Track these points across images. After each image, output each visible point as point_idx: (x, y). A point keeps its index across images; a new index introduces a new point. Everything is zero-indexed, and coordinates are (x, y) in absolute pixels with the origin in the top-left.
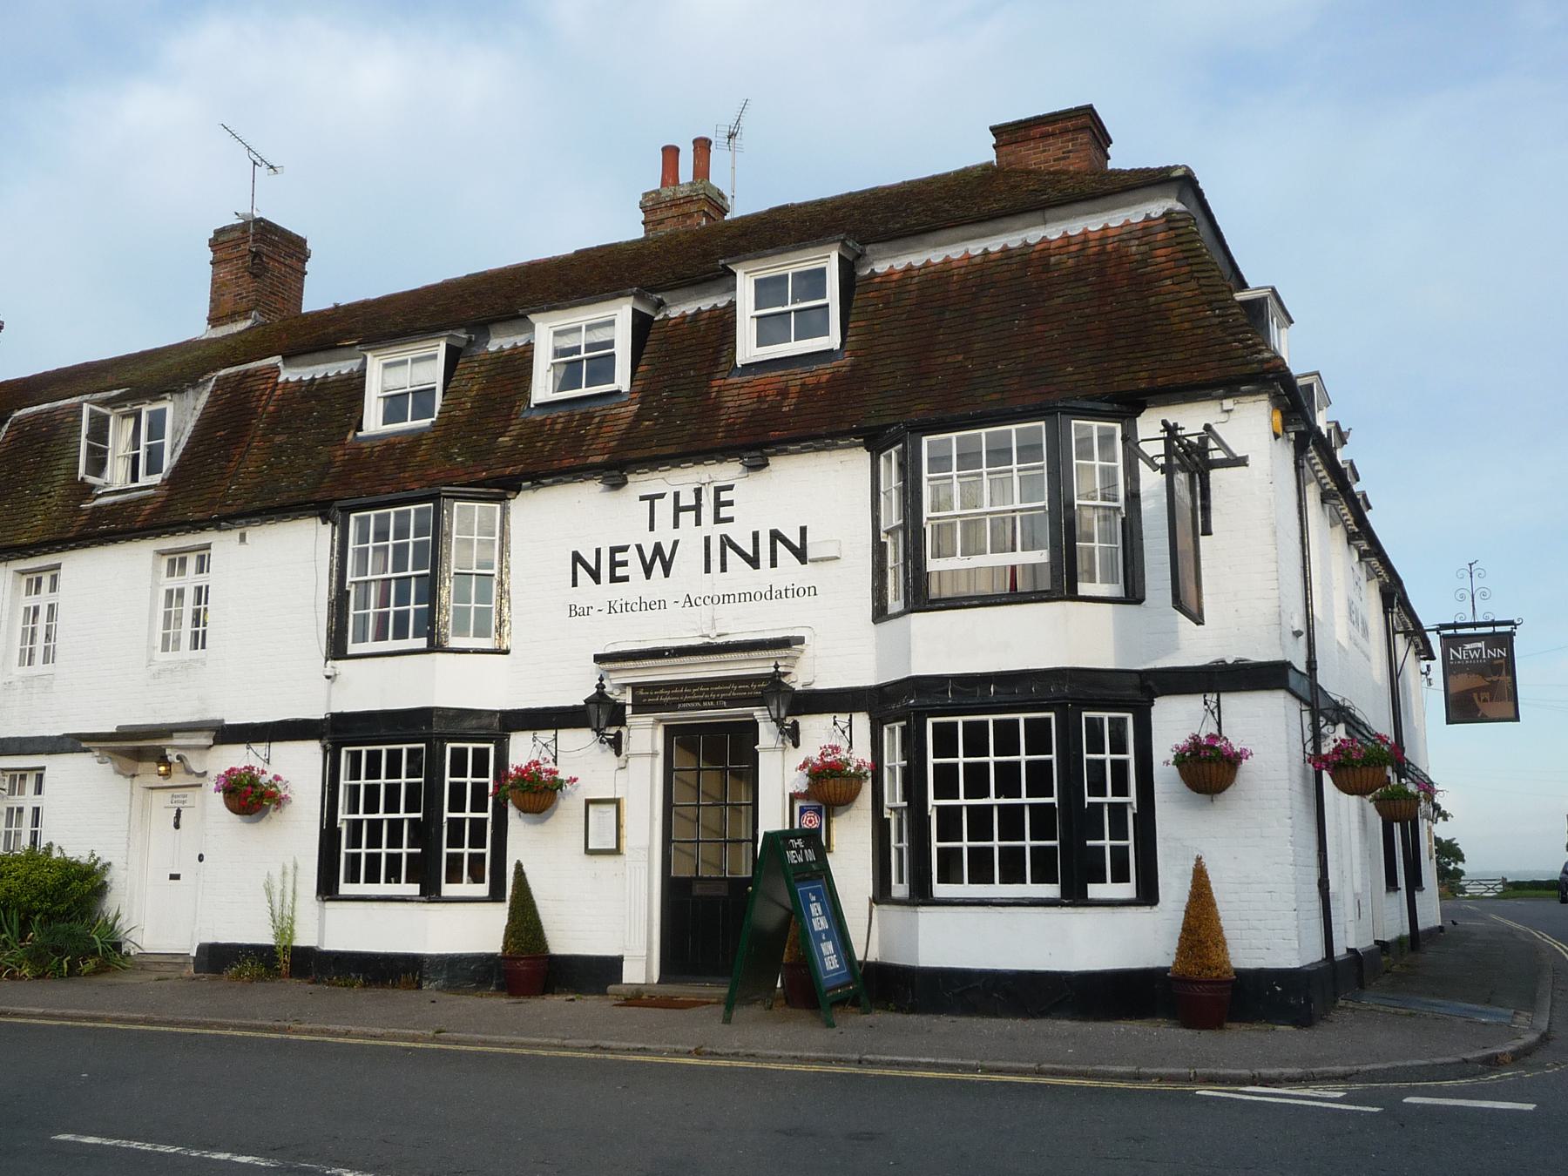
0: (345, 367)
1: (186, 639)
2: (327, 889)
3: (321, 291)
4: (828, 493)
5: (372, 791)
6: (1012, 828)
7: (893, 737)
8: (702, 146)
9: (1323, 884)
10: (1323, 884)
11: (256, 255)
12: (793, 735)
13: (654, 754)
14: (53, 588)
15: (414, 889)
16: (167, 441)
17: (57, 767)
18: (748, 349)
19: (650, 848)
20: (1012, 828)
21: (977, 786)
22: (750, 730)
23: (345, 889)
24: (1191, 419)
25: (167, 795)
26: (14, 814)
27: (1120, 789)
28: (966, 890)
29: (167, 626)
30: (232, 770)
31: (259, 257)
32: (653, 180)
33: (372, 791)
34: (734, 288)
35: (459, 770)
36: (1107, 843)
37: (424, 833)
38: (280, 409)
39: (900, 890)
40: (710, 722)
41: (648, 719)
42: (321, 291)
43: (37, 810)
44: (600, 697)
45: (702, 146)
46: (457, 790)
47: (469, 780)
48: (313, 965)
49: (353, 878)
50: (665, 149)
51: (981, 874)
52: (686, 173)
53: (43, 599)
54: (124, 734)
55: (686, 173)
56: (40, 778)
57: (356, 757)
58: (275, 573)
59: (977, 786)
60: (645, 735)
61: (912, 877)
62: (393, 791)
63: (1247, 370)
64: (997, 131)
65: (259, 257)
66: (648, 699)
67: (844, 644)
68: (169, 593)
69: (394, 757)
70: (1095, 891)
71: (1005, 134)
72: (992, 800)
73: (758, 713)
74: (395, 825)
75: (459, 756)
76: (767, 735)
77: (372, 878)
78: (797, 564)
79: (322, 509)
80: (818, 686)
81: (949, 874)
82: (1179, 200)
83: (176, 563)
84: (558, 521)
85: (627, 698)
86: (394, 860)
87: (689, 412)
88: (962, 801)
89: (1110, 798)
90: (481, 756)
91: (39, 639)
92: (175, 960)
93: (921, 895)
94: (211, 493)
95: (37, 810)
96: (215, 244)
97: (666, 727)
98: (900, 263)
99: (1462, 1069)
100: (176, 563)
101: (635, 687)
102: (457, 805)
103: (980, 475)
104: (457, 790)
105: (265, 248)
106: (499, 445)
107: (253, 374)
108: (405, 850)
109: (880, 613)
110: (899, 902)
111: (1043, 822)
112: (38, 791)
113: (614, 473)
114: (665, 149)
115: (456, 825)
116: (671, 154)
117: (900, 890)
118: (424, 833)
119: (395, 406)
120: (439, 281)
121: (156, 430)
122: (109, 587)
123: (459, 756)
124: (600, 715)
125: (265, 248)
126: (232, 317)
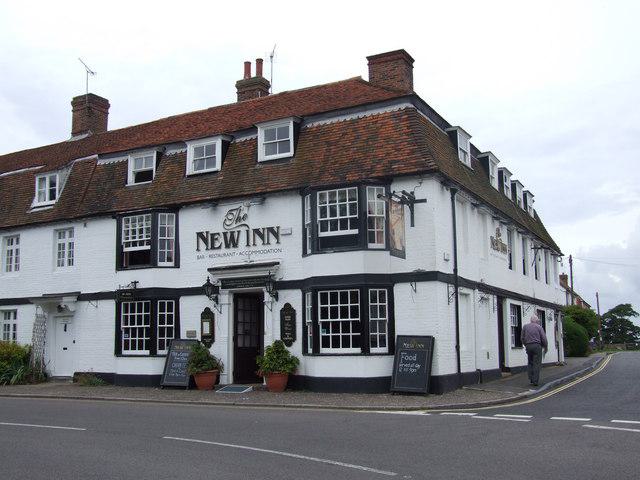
0: (121, 159)
1: (66, 263)
2: (118, 353)
3: (115, 122)
4: (287, 214)
5: (133, 317)
6: (346, 330)
7: (309, 296)
8: (260, 62)
9: (458, 347)
10: (458, 347)
11: (89, 108)
12: (276, 297)
13: (229, 304)
14: (18, 242)
15: (147, 352)
16: (57, 187)
17: (21, 309)
18: (262, 156)
19: (228, 338)
20: (346, 330)
21: (334, 315)
22: (261, 296)
23: (124, 352)
24: (408, 187)
25: (61, 319)
26: (7, 327)
27: (383, 315)
28: (130, 352)
29: (59, 257)
30: (370, 138)
31: (91, 109)
32: (241, 76)
33: (133, 317)
34: (257, 132)
35: (162, 310)
36: (378, 334)
37: (151, 332)
38: (104, 170)
39: (310, 351)
40: (248, 295)
41: (227, 291)
42: (115, 122)
43: (15, 325)
44: (208, 284)
45: (260, 62)
46: (162, 317)
47: (166, 313)
48: (109, 379)
49: (127, 348)
50: (246, 63)
51: (336, 345)
52: (253, 74)
53: (14, 247)
54: (45, 297)
55: (253, 74)
56: (15, 313)
57: (126, 305)
58: (97, 240)
59: (334, 315)
60: (226, 298)
61: (314, 347)
62: (140, 317)
63: (427, 169)
64: (369, 58)
65: (91, 109)
66: (226, 284)
67: (295, 264)
68: (60, 245)
69: (140, 305)
70: (373, 350)
71: (373, 61)
72: (339, 319)
73: (264, 289)
74: (141, 329)
75: (162, 305)
76: (267, 297)
77: (134, 348)
78: (280, 237)
79: (117, 216)
80: (284, 279)
81: (326, 345)
82: (412, 103)
83: (61, 234)
84: (193, 222)
85: (220, 284)
86: (141, 342)
87: (241, 183)
88: (350, 319)
89: (379, 318)
90: (170, 305)
91: (13, 262)
92: (64, 379)
93: (316, 353)
94: (71, 212)
95: (15, 325)
96: (73, 103)
97: (237, 297)
98: (316, 124)
99: (452, 407)
100: (61, 234)
101: (222, 280)
102: (162, 322)
103: (350, 200)
104: (162, 317)
105: (91, 105)
106: (173, 196)
107: (89, 162)
108: (144, 338)
109: (305, 254)
110: (309, 355)
111: (357, 326)
112: (15, 318)
113: (214, 203)
114: (246, 63)
115: (162, 329)
116: (248, 65)
117: (310, 351)
118: (151, 332)
119: (141, 176)
120: (206, 107)
121: (53, 184)
122: (37, 244)
123: (162, 305)
124: (208, 290)
125: (91, 105)
126: (85, 132)
